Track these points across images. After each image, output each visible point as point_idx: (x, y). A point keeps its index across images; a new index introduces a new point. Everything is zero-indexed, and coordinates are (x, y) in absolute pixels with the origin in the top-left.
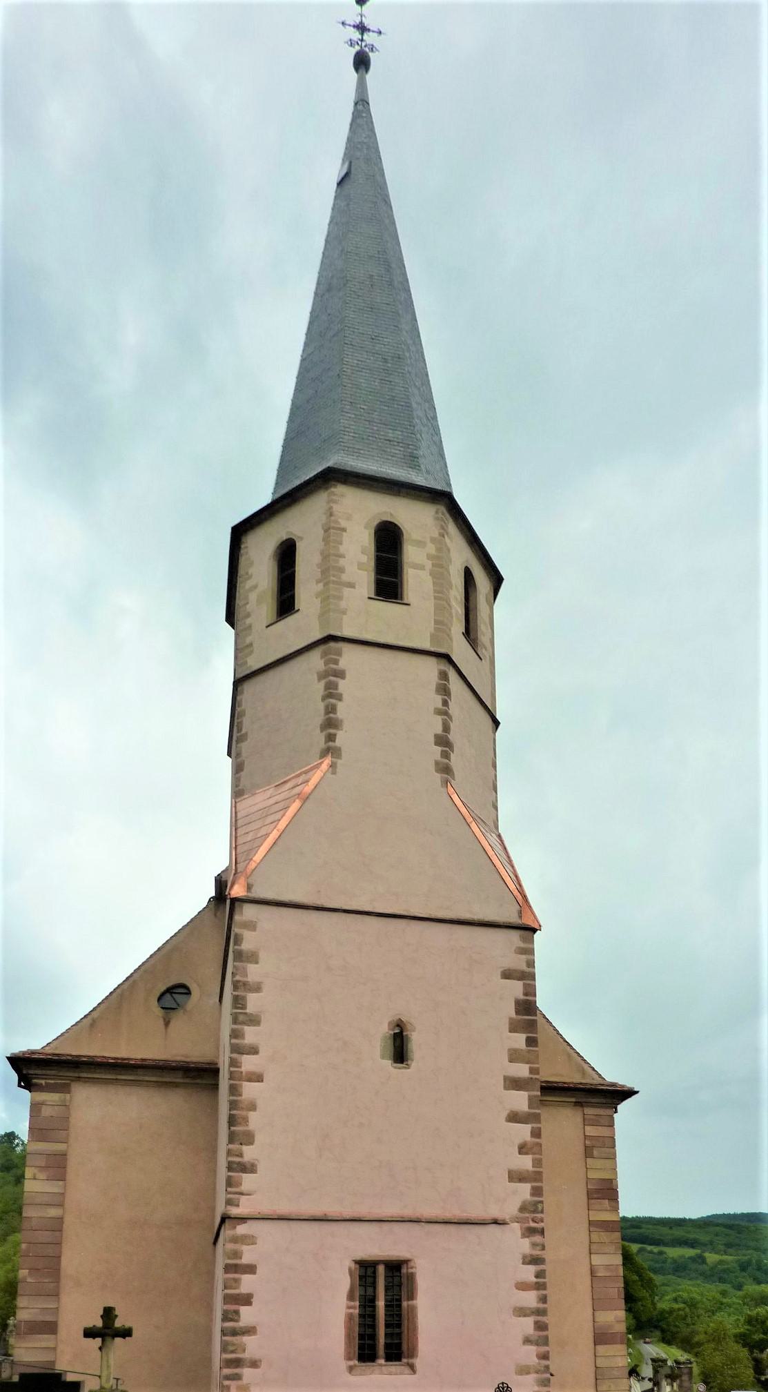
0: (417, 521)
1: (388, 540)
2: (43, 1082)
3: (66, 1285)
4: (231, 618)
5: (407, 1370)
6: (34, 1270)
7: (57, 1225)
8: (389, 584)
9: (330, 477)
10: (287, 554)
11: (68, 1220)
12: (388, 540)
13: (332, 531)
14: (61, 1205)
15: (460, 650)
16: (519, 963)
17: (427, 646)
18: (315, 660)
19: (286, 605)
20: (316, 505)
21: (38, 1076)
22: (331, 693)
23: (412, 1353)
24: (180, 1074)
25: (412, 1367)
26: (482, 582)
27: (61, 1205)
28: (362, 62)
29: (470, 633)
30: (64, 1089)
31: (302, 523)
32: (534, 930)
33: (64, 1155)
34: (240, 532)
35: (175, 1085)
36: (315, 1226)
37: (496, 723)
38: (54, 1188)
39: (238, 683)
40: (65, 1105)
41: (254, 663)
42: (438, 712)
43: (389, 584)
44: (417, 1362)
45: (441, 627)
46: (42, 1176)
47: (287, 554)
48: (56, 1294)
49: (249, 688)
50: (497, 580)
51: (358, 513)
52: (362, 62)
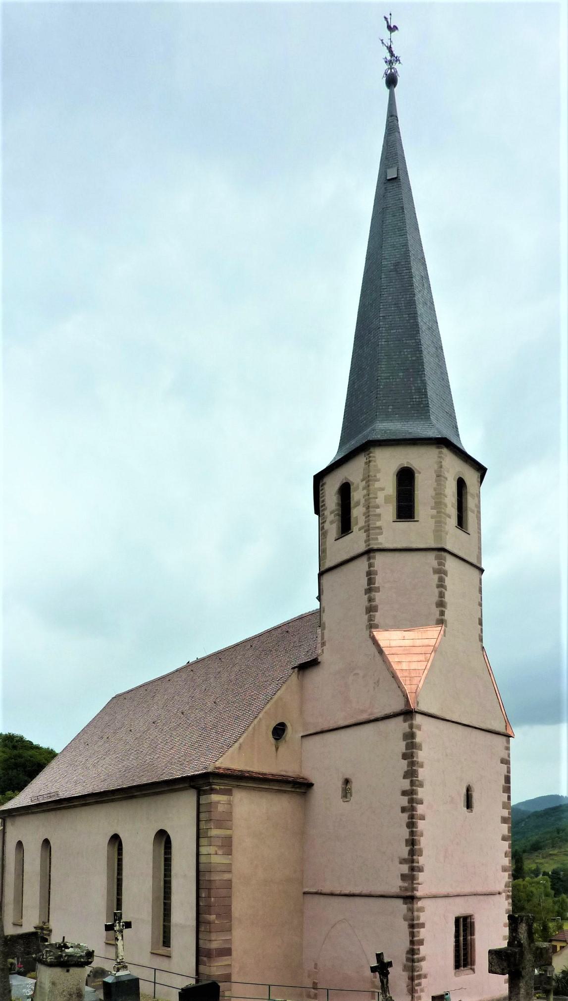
0: (423, 461)
1: (406, 477)
2: (218, 787)
3: (235, 923)
4: (317, 511)
6: (218, 915)
7: (229, 884)
8: (406, 509)
10: (345, 490)
12: (406, 477)
13: (368, 479)
14: (230, 872)
16: (503, 754)
17: (433, 546)
18: (362, 565)
19: (346, 527)
20: (359, 463)
22: (371, 589)
23: (473, 963)
25: (473, 970)
26: (471, 477)
29: (461, 523)
30: (228, 792)
31: (353, 472)
32: (509, 736)
33: (230, 838)
34: (319, 479)
36: (382, 900)
39: (321, 575)
40: (230, 803)
41: (329, 564)
42: (405, 756)
43: (406, 509)
44: (476, 967)
45: (439, 530)
46: (220, 852)
47: (345, 490)
48: (229, 930)
49: (326, 577)
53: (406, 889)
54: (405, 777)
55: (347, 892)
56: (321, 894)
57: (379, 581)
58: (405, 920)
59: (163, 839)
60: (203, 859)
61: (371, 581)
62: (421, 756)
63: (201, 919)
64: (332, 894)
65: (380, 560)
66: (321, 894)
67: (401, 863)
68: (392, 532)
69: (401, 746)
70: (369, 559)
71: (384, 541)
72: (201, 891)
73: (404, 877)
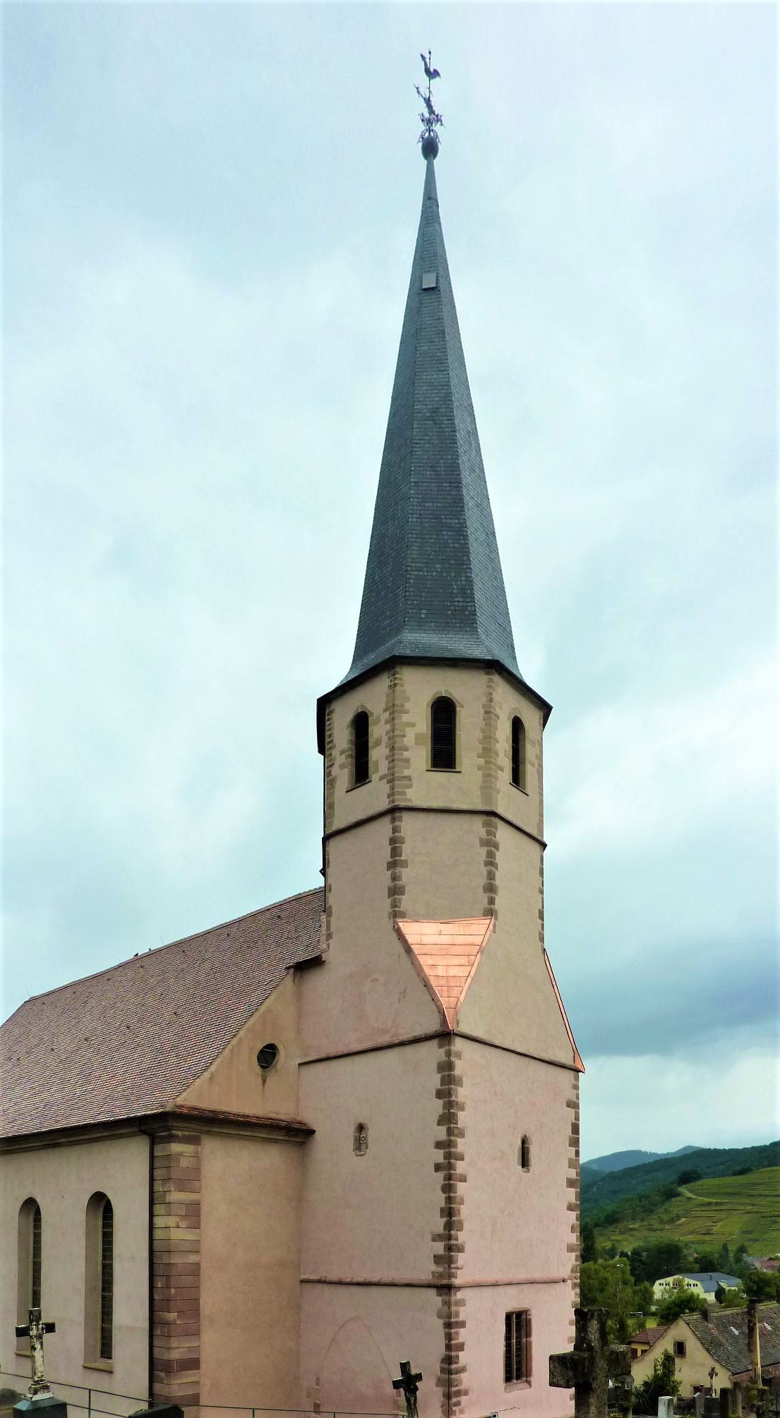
0: (467, 690)
1: (444, 711)
2: (180, 1133)
3: (204, 1323)
4: (322, 749)
5: (526, 1385)
6: (181, 1313)
7: (195, 1270)
9: (391, 664)
10: (361, 723)
11: (204, 1265)
12: (444, 711)
13: (393, 709)
15: (506, 800)
19: (361, 774)
20: (381, 685)
21: (178, 1128)
23: (528, 1374)
24: (283, 1132)
25: (529, 1383)
26: (530, 717)
27: (197, 1252)
28: (430, 148)
29: (517, 779)
31: (373, 698)
34: (324, 704)
35: (276, 1141)
37: (544, 846)
38: (189, 1235)
39: (326, 840)
40: (197, 1156)
45: (488, 786)
46: (183, 1224)
47: (361, 723)
48: (197, 1333)
49: (332, 843)
50: (545, 709)
51: (419, 690)
52: (430, 148)
53: (441, 1276)
54: (439, 1124)
55: (361, 1279)
56: (325, 1282)
57: (406, 851)
58: (439, 1316)
59: (101, 1205)
60: (158, 1234)
61: (395, 852)
62: (462, 1094)
63: (156, 1319)
64: (340, 1283)
65: (408, 823)
66: (325, 1282)
67: (434, 1240)
68: (425, 785)
69: (435, 1081)
70: (393, 820)
71: (414, 796)
72: (156, 1278)
73: (438, 1259)
